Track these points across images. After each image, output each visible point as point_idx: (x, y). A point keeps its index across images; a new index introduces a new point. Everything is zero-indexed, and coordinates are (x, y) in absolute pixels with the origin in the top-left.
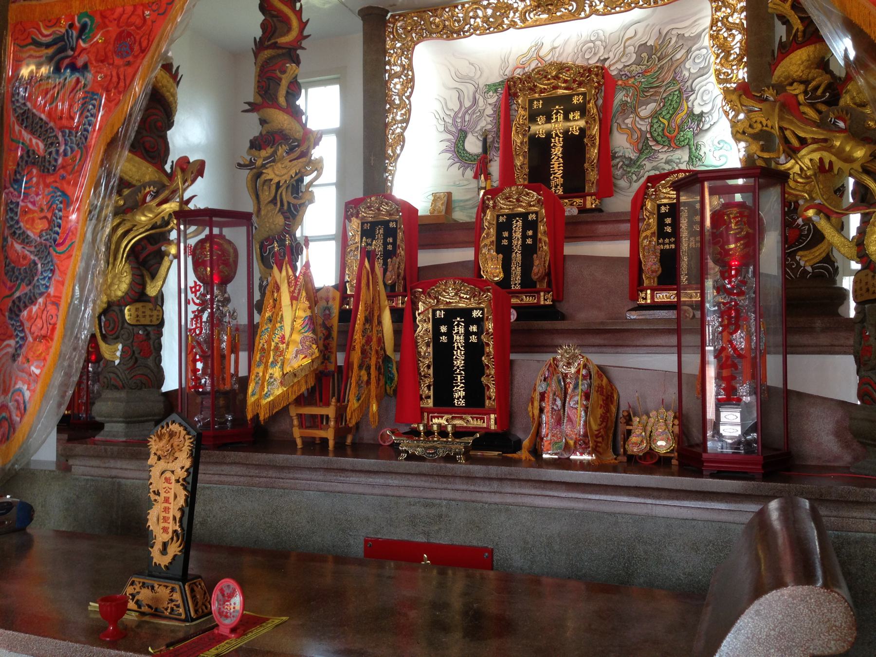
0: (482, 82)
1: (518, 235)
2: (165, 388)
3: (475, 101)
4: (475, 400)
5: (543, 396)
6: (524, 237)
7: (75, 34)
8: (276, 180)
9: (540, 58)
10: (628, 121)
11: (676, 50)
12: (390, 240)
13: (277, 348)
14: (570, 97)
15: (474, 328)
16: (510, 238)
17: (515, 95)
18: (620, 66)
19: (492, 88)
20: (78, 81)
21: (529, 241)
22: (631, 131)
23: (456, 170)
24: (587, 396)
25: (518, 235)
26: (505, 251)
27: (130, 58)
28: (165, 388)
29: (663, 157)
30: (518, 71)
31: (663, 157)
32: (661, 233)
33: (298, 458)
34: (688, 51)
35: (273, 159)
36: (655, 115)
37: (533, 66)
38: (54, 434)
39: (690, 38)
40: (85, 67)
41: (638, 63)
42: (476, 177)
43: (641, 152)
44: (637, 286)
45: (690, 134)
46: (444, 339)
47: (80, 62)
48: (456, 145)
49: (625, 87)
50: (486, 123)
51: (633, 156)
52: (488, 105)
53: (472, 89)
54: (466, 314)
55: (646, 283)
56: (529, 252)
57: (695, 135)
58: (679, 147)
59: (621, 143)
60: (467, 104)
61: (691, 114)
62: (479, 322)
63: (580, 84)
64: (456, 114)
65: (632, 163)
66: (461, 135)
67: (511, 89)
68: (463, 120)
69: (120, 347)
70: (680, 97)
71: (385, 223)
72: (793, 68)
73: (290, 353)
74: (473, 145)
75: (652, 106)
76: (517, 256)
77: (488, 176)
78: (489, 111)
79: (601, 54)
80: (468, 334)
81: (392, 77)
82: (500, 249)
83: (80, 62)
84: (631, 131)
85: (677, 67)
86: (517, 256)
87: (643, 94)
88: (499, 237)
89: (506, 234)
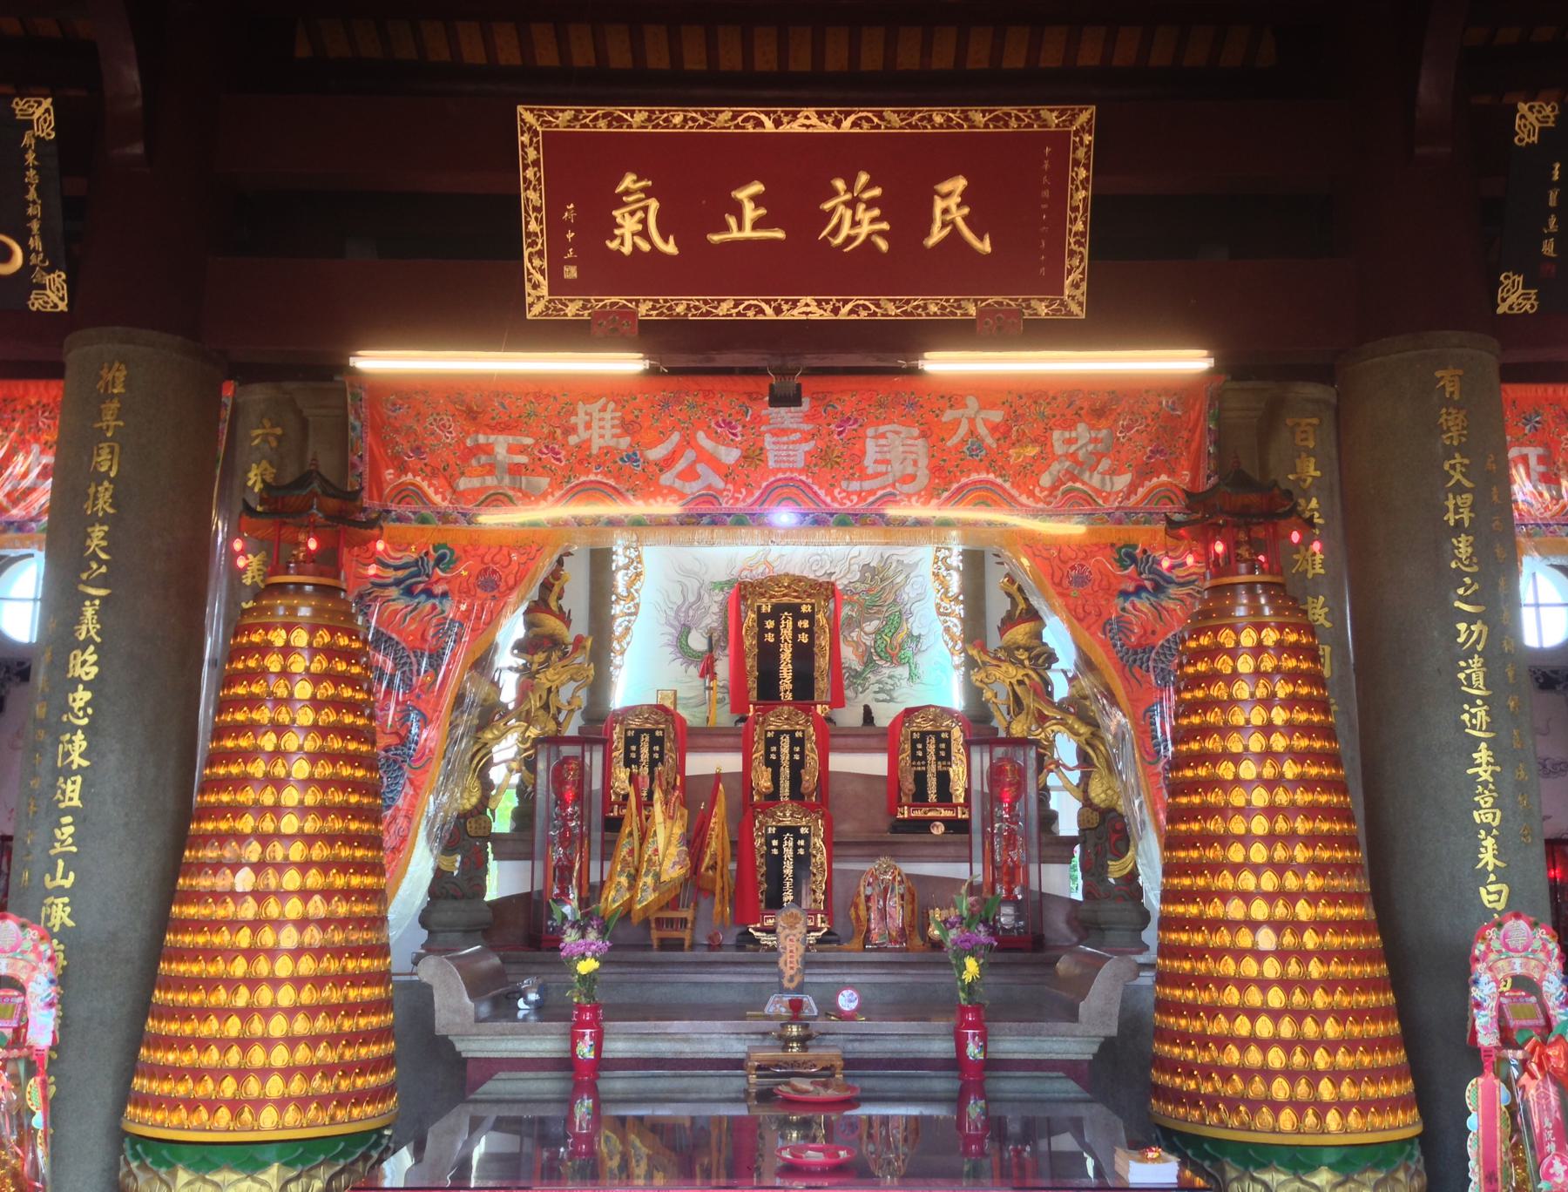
0: (707, 579)
1: (785, 749)
2: (487, 899)
3: (700, 597)
4: (1169, 896)
5: (868, 898)
6: (792, 753)
7: (432, 563)
8: (548, 685)
9: (768, 564)
10: (854, 634)
11: (896, 574)
12: (657, 748)
13: (650, 860)
14: (799, 605)
15: (801, 843)
16: (778, 753)
17: (745, 598)
18: (846, 582)
19: (721, 586)
20: (434, 607)
21: (797, 757)
22: (857, 644)
23: (678, 666)
24: (902, 897)
25: (785, 749)
26: (775, 766)
27: (495, 593)
28: (487, 899)
29: (886, 671)
30: (745, 573)
31: (886, 671)
32: (914, 757)
33: (655, 955)
34: (907, 577)
35: (547, 663)
36: (879, 632)
37: (761, 570)
38: (391, 943)
39: (908, 565)
40: (444, 595)
41: (862, 580)
42: (702, 675)
43: (866, 665)
44: (895, 802)
45: (909, 654)
46: (775, 852)
47: (438, 589)
48: (679, 639)
49: (850, 602)
50: (712, 619)
51: (859, 668)
52: (714, 605)
53: (697, 584)
54: (794, 831)
55: (904, 799)
56: (797, 767)
57: (914, 654)
58: (900, 664)
59: (848, 654)
60: (692, 599)
61: (910, 635)
62: (807, 837)
63: (809, 596)
64: (679, 608)
65: (857, 674)
66: (685, 630)
67: (742, 591)
68: (687, 612)
69: (459, 858)
70: (900, 617)
71: (651, 732)
72: (1020, 637)
73: (667, 864)
74: (698, 642)
75: (876, 623)
76: (785, 771)
77: (714, 676)
78: (715, 608)
79: (828, 568)
80: (796, 847)
81: (618, 569)
82: (768, 762)
83: (438, 589)
84: (857, 644)
85: (897, 590)
86: (785, 771)
87: (867, 611)
88: (768, 752)
89: (774, 749)
